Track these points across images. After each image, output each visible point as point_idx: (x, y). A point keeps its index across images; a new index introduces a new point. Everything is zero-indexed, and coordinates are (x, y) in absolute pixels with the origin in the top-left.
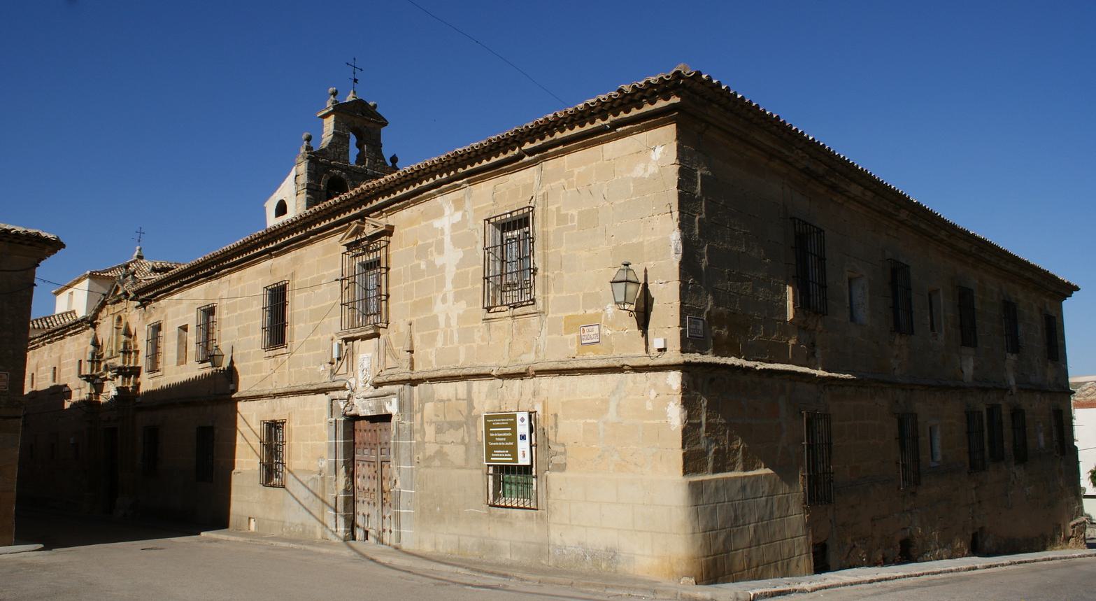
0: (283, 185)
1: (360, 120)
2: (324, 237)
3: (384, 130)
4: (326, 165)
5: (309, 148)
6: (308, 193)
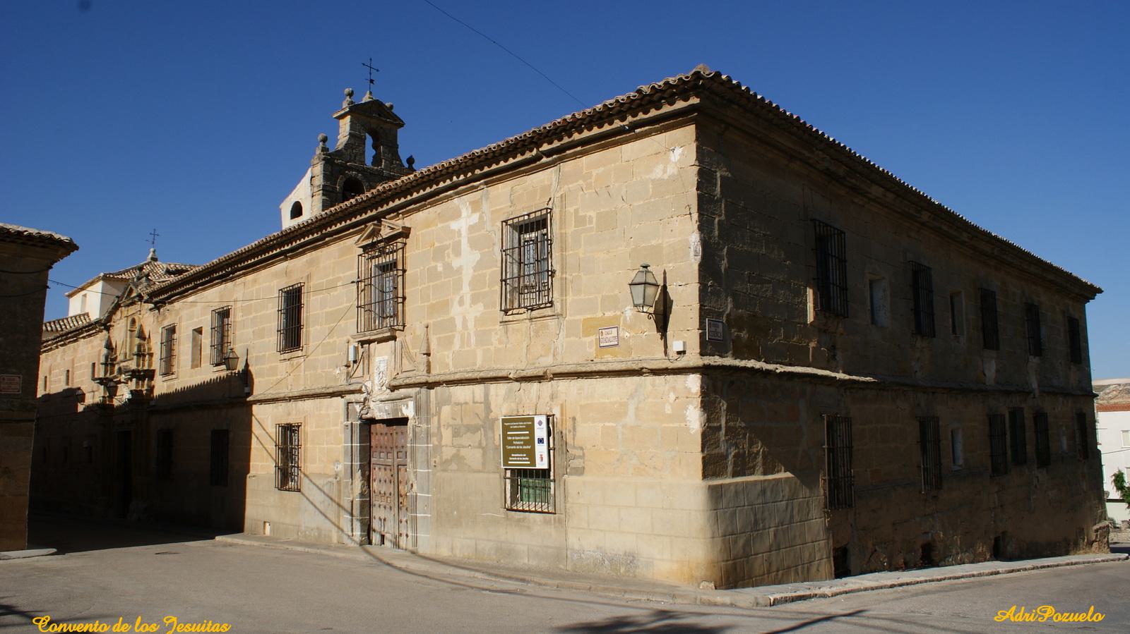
0: (298, 186)
1: (377, 121)
3: (400, 132)
5: (324, 149)
6: (323, 195)
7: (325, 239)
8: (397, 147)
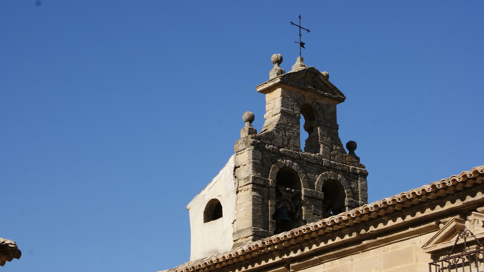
0: (215, 180)
1: (312, 97)
2: (387, 242)
3: (340, 108)
4: (273, 153)
5: (252, 131)
6: (254, 190)
7: (361, 242)
8: (336, 127)
